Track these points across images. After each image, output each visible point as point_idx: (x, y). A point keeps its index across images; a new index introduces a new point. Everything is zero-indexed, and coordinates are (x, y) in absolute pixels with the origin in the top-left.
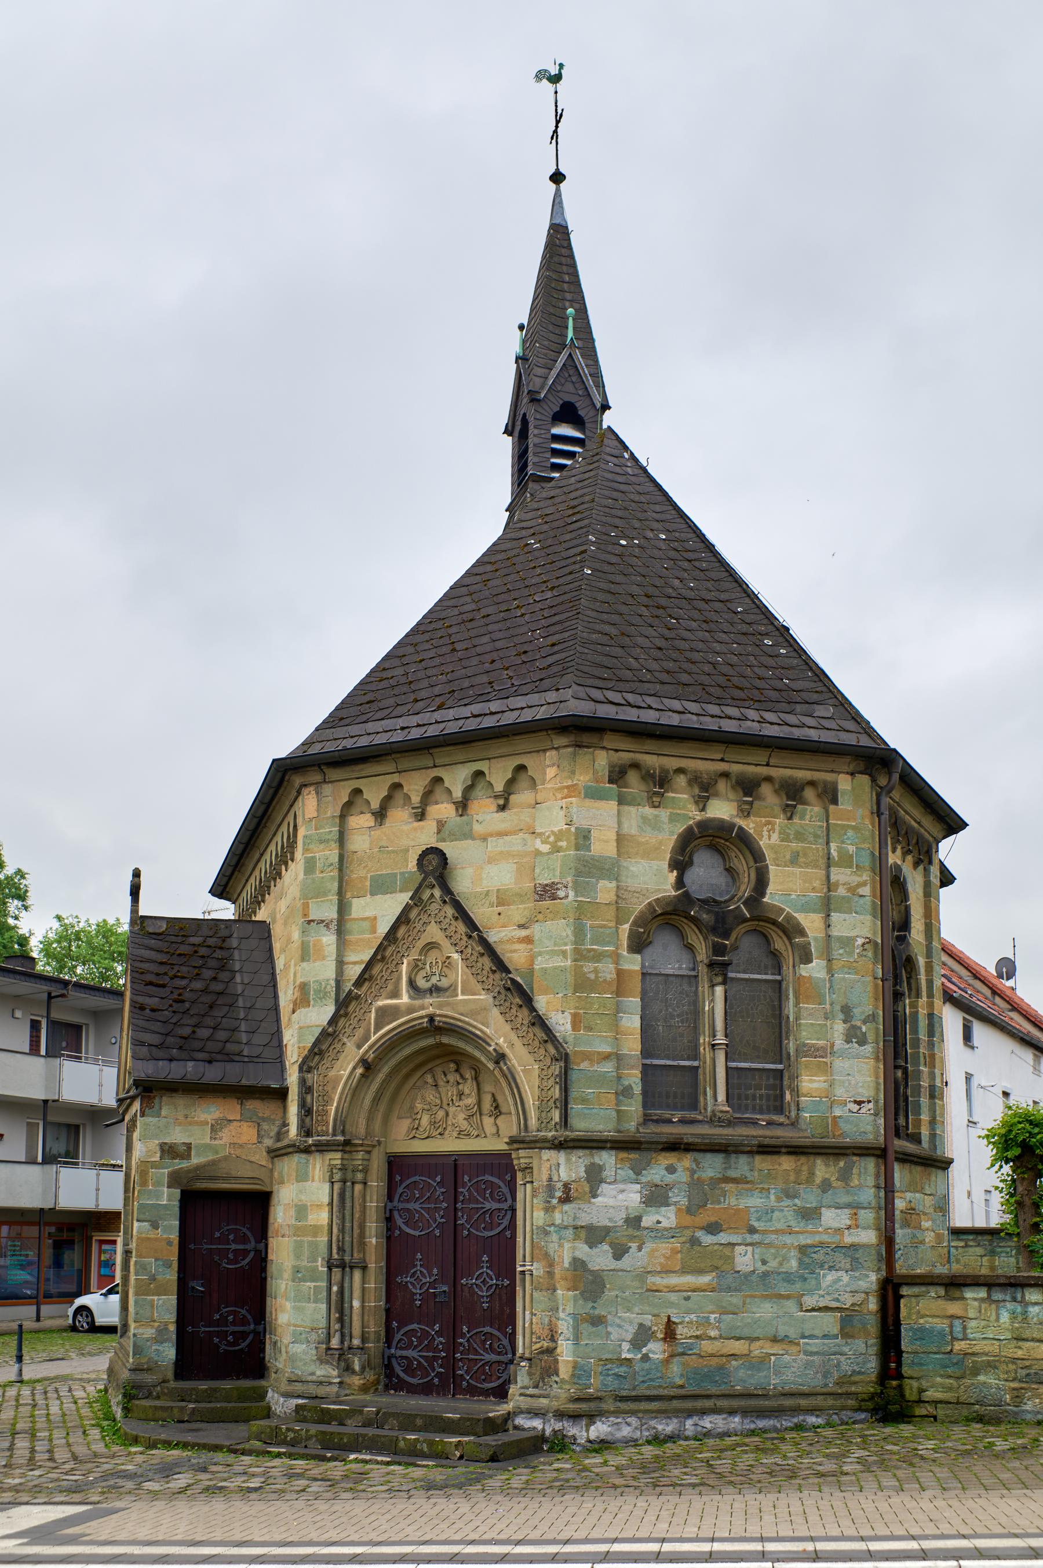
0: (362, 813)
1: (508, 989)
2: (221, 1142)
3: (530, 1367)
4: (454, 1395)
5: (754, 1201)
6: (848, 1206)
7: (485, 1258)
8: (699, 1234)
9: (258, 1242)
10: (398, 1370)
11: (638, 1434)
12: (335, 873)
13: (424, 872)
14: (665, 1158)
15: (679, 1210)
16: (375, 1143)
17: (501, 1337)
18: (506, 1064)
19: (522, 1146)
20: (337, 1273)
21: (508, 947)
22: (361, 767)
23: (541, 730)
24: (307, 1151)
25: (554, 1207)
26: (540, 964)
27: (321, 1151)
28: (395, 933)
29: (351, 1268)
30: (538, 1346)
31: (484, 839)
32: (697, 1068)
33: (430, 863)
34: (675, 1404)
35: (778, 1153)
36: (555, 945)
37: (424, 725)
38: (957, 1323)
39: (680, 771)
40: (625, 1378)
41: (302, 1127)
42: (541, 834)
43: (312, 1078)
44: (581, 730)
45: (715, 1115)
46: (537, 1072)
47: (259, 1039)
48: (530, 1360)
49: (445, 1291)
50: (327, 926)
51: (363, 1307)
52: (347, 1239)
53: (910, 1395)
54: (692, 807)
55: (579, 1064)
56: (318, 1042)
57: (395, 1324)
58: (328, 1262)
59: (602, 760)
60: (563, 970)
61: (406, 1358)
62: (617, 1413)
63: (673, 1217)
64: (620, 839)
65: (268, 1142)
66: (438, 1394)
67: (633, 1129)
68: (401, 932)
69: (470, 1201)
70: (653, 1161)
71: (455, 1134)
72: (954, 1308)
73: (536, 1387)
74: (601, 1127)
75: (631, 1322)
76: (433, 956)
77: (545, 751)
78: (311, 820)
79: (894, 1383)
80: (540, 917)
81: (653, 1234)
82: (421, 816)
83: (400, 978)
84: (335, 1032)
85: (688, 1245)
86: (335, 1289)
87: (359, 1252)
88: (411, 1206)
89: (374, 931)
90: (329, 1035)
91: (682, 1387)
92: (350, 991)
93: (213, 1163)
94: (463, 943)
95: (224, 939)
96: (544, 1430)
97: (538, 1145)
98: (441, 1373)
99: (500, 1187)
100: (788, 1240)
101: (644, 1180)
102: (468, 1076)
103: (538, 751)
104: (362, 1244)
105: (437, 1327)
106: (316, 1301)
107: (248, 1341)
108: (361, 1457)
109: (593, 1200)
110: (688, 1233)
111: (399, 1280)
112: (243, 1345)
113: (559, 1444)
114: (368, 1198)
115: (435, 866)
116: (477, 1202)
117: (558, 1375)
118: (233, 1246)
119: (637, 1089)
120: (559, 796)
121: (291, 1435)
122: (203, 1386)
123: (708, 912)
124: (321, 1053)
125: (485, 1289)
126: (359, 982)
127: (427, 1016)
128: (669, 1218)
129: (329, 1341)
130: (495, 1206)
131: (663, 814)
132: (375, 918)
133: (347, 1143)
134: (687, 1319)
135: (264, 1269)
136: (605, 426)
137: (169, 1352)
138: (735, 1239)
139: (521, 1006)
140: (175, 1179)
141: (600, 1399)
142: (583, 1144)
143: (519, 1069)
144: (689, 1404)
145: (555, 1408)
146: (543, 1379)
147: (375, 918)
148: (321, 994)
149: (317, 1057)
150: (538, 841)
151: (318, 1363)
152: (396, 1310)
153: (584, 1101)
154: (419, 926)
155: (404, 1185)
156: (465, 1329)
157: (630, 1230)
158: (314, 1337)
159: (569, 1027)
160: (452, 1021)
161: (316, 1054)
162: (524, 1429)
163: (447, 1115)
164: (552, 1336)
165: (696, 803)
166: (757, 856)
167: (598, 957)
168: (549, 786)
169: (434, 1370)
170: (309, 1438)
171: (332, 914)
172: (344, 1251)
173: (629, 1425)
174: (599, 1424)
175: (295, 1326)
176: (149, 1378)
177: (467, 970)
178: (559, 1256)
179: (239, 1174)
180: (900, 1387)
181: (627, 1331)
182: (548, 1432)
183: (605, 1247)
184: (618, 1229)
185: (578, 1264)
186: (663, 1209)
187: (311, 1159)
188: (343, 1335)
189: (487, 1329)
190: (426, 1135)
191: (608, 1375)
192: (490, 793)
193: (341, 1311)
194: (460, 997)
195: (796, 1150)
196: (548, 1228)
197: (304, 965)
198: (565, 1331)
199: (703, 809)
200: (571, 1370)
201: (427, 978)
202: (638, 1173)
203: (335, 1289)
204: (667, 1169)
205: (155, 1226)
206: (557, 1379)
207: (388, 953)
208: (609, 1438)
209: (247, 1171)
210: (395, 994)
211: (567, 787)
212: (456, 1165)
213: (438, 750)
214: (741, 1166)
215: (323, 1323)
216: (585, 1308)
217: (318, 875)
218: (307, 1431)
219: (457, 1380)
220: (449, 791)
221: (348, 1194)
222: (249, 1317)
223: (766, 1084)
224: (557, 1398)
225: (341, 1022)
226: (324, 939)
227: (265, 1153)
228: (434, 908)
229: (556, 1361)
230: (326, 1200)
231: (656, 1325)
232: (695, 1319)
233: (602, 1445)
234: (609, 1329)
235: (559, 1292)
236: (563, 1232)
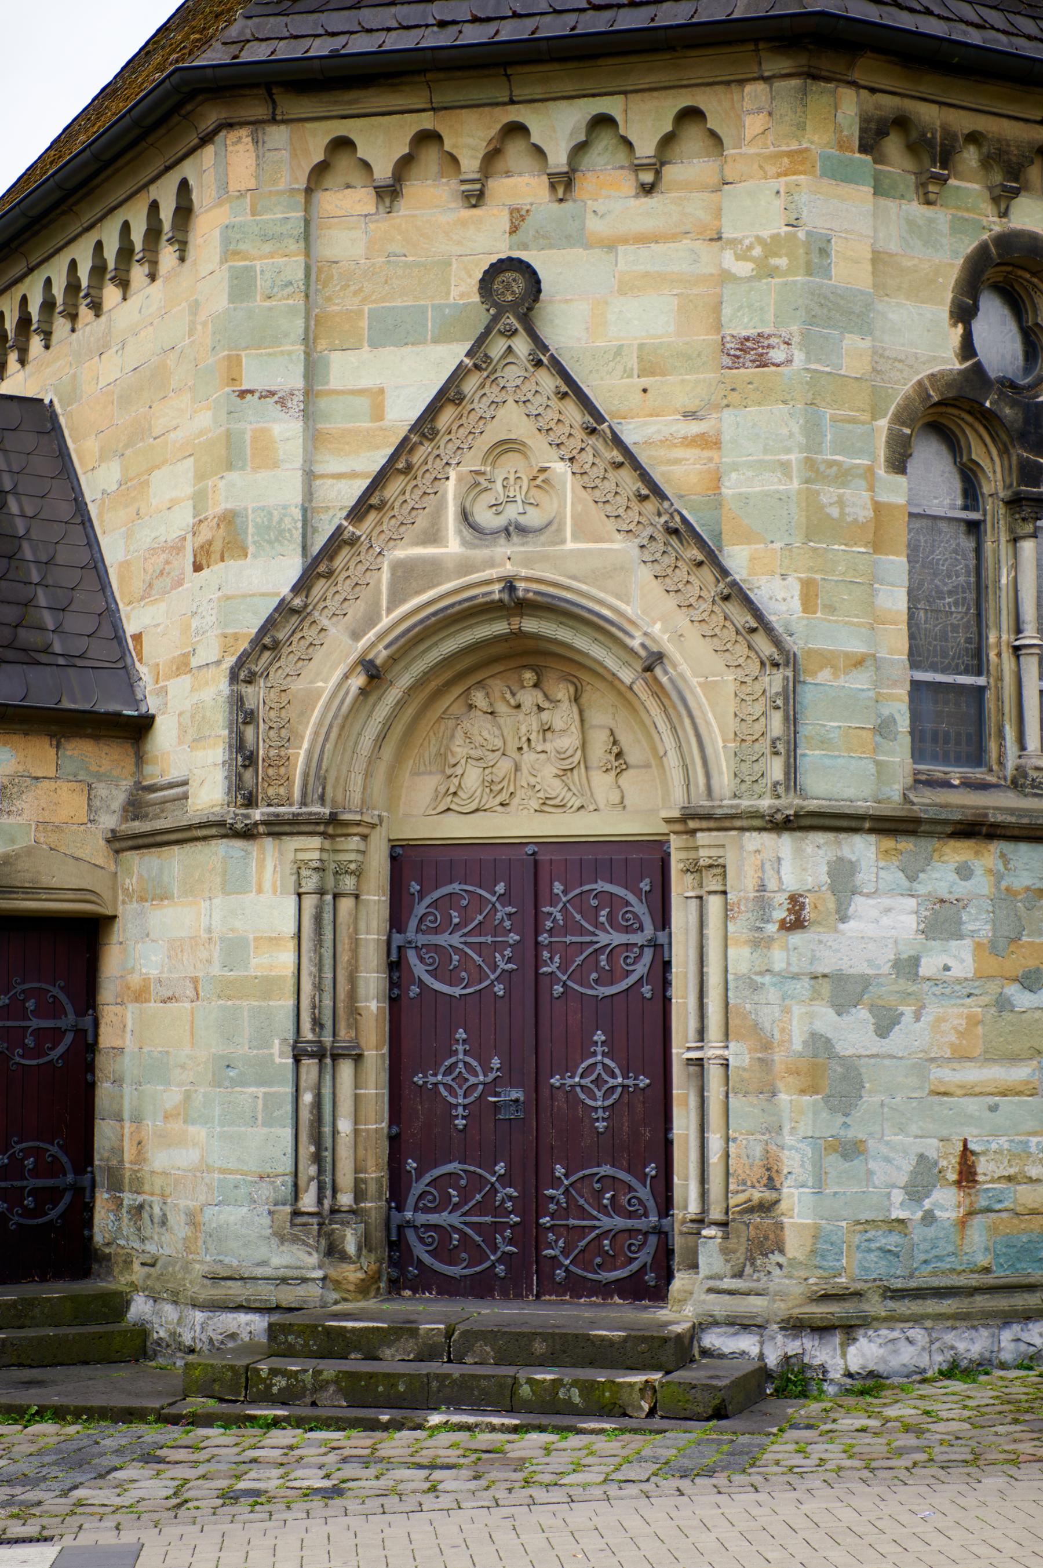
0: (348, 187)
1: (675, 532)
2: (20, 820)
3: (726, 1237)
4: (538, 1296)
7: (599, 1036)
8: (1013, 990)
9: (80, 1013)
10: (420, 1252)
11: (924, 1362)
12: (299, 301)
13: (495, 304)
14: (955, 850)
15: (978, 946)
16: (376, 821)
17: (634, 1183)
18: (666, 672)
19: (704, 824)
20: (310, 1065)
21: (662, 453)
22: (353, 94)
23: (743, 41)
24: (247, 834)
25: (771, 939)
26: (732, 486)
28: (433, 420)
29: (335, 1057)
30: (741, 1198)
32: (981, 690)
33: (508, 287)
34: (981, 1302)
36: (765, 451)
37: (489, 20)
39: (974, 138)
40: (897, 1255)
41: (239, 788)
42: (733, 242)
43: (254, 695)
44: (817, 48)
45: (1025, 776)
46: (731, 687)
47: (75, 623)
48: (724, 1224)
49: (517, 1101)
50: (282, 402)
51: (356, 1132)
52: (328, 1002)
54: (988, 208)
55: (814, 674)
56: (269, 625)
57: (412, 1164)
58: (294, 1048)
59: (849, 107)
60: (782, 499)
61: (436, 1227)
62: (891, 1320)
63: (967, 956)
64: (877, 258)
65: (109, 821)
66: (505, 1295)
67: (897, 797)
68: (446, 418)
69: (566, 930)
70: (936, 855)
71: (535, 804)
73: (739, 1275)
74: (850, 792)
75: (906, 1153)
76: (510, 465)
77: (742, 82)
78: (241, 195)
80: (734, 397)
81: (937, 990)
82: (476, 198)
83: (441, 506)
84: (306, 606)
85: (993, 1010)
86: (307, 1098)
87: (349, 1026)
88: (442, 939)
89: (378, 413)
90: (294, 611)
91: (987, 1270)
92: (340, 529)
94: (575, 443)
96: (761, 1356)
97: (738, 823)
98: (511, 1254)
99: (628, 903)
101: (922, 889)
102: (560, 695)
103: (728, 83)
104: (354, 1012)
105: (500, 1168)
106: (268, 1123)
107: (62, 1206)
108: (456, 1419)
109: (841, 926)
110: (993, 987)
111: (418, 1079)
112: (53, 1214)
113: (793, 1382)
114: (362, 925)
115: (513, 291)
116: (582, 931)
117: (782, 1251)
118: (35, 1023)
119: (904, 724)
120: (772, 170)
121: (280, 1382)
123: (1014, 404)
124: (275, 646)
125: (599, 1094)
126: (359, 510)
127: (499, 580)
128: (962, 961)
129: (296, 1198)
130: (618, 938)
131: (940, 217)
132: (382, 391)
133: (333, 819)
134: (994, 1146)
135: (90, 1067)
139: (700, 564)
141: (858, 1294)
142: (827, 822)
143: (694, 681)
144: (1002, 1303)
145: (784, 1314)
146: (752, 1261)
147: (382, 391)
149: (267, 654)
151: (274, 1241)
152: (411, 1130)
153: (824, 743)
154: (481, 407)
155: (427, 901)
156: (560, 1170)
157: (901, 981)
158: (265, 1191)
159: (796, 604)
160: (551, 590)
161: (265, 647)
162: (722, 1356)
163: (517, 768)
164: (770, 1179)
165: (995, 200)
167: (843, 476)
168: (752, 151)
169: (495, 1249)
170: (320, 1386)
172: (322, 1026)
173: (910, 1341)
174: (863, 1341)
175: (222, 1171)
177: (584, 494)
178: (783, 1030)
179: (54, 883)
181: (899, 1168)
182: (772, 1360)
183: (862, 1013)
184: (882, 980)
185: (820, 1045)
186: (954, 943)
187: (253, 847)
188: (321, 1189)
189: (606, 1170)
190: (473, 806)
191: (869, 1250)
192: (621, 157)
193: (317, 1139)
194: (570, 545)
196: (758, 979)
197: (233, 476)
198: (797, 1170)
199: (1004, 214)
200: (809, 1242)
202: (912, 878)
203: (307, 1098)
204: (958, 871)
206: (781, 1259)
207: (417, 458)
208: (881, 1368)
209: (62, 875)
210: (433, 536)
211: (790, 154)
212: (536, 862)
213: (520, 69)
215: (288, 1166)
216: (832, 1126)
217: (259, 302)
218: (317, 1373)
219: (545, 1267)
220: (539, 151)
221: (328, 917)
222: (64, 1159)
224: (782, 1295)
225: (320, 587)
227: (102, 843)
228: (512, 374)
229: (780, 1226)
230: (291, 928)
231: (945, 1157)
232: (1006, 1146)
233: (869, 1385)
234: (872, 1165)
235: (783, 1097)
236: (791, 986)
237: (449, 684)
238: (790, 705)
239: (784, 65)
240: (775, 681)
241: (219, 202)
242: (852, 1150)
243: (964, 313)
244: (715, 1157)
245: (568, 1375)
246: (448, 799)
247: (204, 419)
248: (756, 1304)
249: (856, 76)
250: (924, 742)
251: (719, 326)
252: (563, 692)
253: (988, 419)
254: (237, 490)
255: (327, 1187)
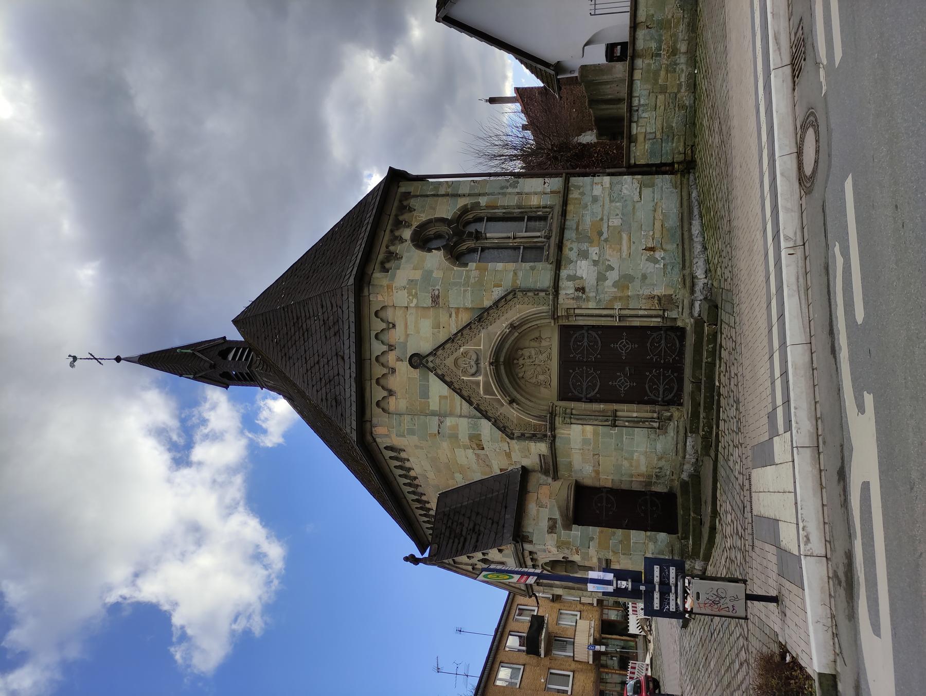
5: (588, 220)
6: (592, 186)
8: (602, 238)
10: (670, 396)
12: (416, 417)
24: (554, 437)
27: (555, 429)
31: (407, 336)
35: (566, 211)
38: (647, 137)
43: (517, 433)
44: (362, 281)
53: (680, 158)
56: (498, 428)
65: (550, 480)
68: (448, 379)
72: (641, 138)
79: (676, 166)
89: (446, 397)
93: (559, 508)
95: (445, 515)
100: (607, 206)
105: (648, 374)
106: (633, 435)
115: (417, 361)
118: (604, 504)
119: (532, 264)
122: (680, 512)
124: (504, 427)
126: (470, 403)
130: (586, 339)
131: (405, 255)
133: (551, 414)
136: (235, 335)
137: (662, 536)
138: (605, 226)
140: (568, 527)
148: (475, 426)
150: (411, 305)
152: (637, 397)
158: (653, 436)
166: (429, 222)
167: (468, 277)
171: (435, 420)
176: (677, 546)
180: (679, 163)
182: (702, 297)
185: (615, 285)
187: (558, 435)
189: (648, 345)
192: (386, 332)
193: (638, 422)
195: (565, 203)
201: (471, 367)
205: (592, 539)
209: (564, 494)
210: (478, 383)
214: (571, 223)
216: (637, 283)
220: (383, 353)
223: (535, 217)
225: (490, 414)
226: (448, 424)
236: (600, 291)
237: (517, 383)
238: (525, 291)
239: (366, 290)
240: (519, 295)
241: (390, 437)
242: (644, 277)
243: (430, 250)
244: (646, 313)
245: (705, 348)
246: (547, 384)
247: (445, 445)
248: (686, 302)
249: (370, 273)
250: (538, 260)
251: (428, 308)
252: (520, 352)
253: (456, 244)
254: (464, 437)
255: (652, 419)
